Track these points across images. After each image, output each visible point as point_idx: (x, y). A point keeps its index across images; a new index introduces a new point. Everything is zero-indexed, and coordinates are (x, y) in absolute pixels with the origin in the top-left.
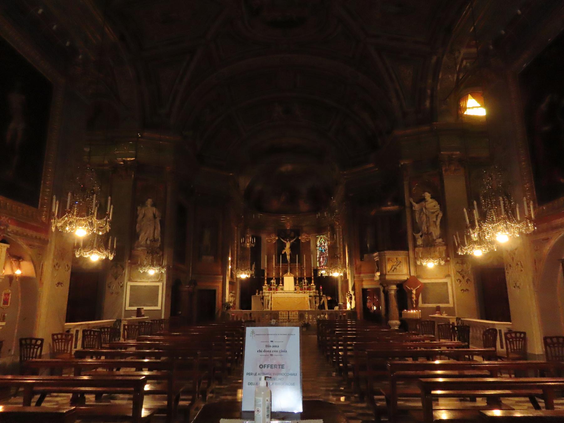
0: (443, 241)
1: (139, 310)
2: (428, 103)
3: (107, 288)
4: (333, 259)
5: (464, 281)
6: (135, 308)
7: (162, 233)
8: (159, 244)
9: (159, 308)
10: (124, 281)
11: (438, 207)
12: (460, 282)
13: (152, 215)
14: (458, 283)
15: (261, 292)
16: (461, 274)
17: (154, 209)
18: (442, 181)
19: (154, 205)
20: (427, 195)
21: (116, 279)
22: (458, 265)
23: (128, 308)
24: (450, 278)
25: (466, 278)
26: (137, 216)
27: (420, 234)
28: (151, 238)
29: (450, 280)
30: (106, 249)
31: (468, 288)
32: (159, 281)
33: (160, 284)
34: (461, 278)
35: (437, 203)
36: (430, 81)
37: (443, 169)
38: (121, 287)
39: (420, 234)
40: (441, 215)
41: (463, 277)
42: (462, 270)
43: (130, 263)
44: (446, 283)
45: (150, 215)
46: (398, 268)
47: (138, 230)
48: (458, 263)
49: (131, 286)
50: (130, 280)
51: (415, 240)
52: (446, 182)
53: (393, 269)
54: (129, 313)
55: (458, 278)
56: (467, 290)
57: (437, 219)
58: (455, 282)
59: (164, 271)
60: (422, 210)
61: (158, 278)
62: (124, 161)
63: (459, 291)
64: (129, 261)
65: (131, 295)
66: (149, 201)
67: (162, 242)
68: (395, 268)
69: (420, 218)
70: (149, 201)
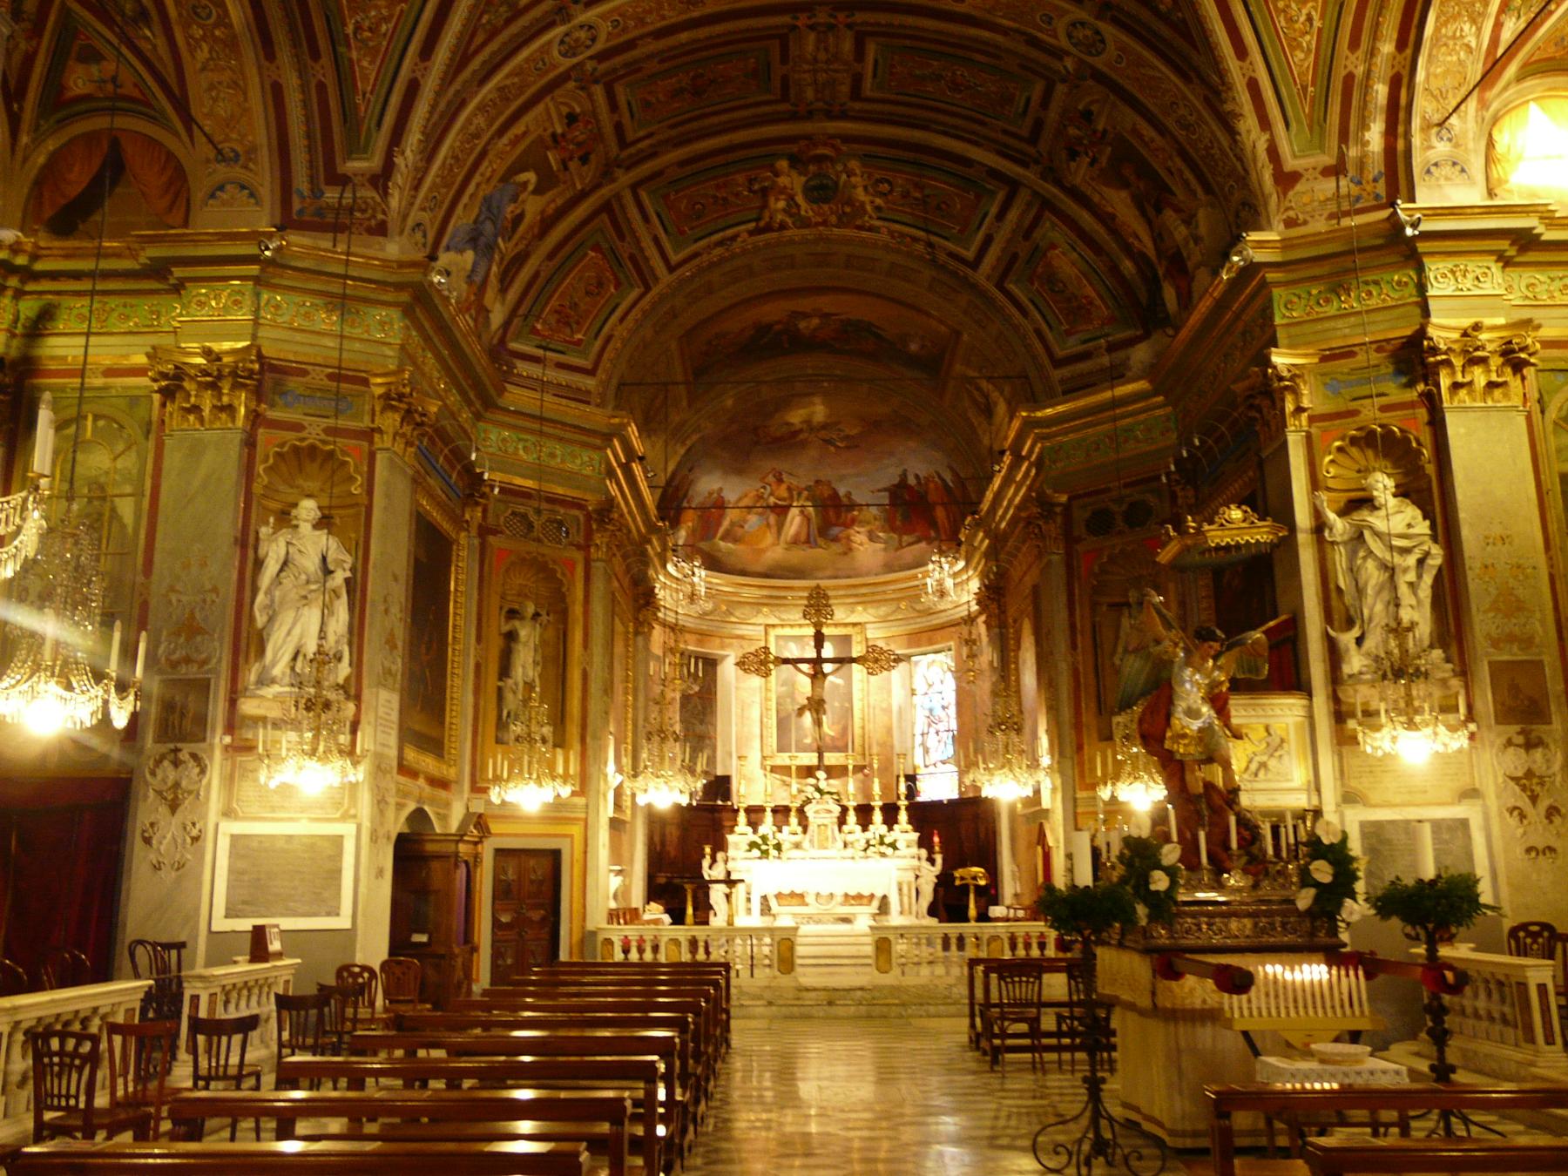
0: (1448, 660)
1: (259, 934)
2: (1375, 136)
3: (138, 843)
4: (1193, 713)
5: (1536, 814)
6: (246, 924)
7: (356, 631)
8: (344, 670)
9: (343, 922)
10: (204, 817)
11: (1423, 527)
12: (1522, 816)
13: (317, 560)
14: (1513, 821)
15: (720, 856)
16: (1524, 788)
17: (322, 535)
18: (1437, 423)
19: (324, 522)
20: (1383, 485)
21: (174, 807)
22: (1511, 750)
23: (221, 924)
24: (1480, 802)
25: (1544, 804)
26: (259, 564)
27: (1356, 632)
28: (311, 647)
29: (1479, 809)
30: (554, 778)
31: (1552, 844)
32: (345, 817)
33: (347, 830)
34: (1524, 802)
35: (1418, 513)
36: (1387, 48)
37: (1445, 381)
38: (195, 839)
39: (1356, 632)
40: (1437, 557)
41: (1534, 799)
42: (1529, 774)
43: (226, 748)
44: (1464, 824)
45: (311, 564)
46: (1272, 763)
47: (260, 620)
48: (1509, 743)
49: (235, 839)
50: (228, 813)
51: (1334, 655)
52: (1455, 426)
53: (1254, 767)
54: (222, 946)
55: (1511, 803)
56: (1551, 849)
57: (1420, 576)
58: (1500, 814)
59: (359, 774)
60: (1359, 538)
61: (337, 805)
62: (207, 353)
63: (1519, 851)
64: (228, 739)
65: (231, 870)
66: (308, 509)
67: (357, 664)
68: (1263, 765)
69: (1353, 571)
70: (308, 509)
